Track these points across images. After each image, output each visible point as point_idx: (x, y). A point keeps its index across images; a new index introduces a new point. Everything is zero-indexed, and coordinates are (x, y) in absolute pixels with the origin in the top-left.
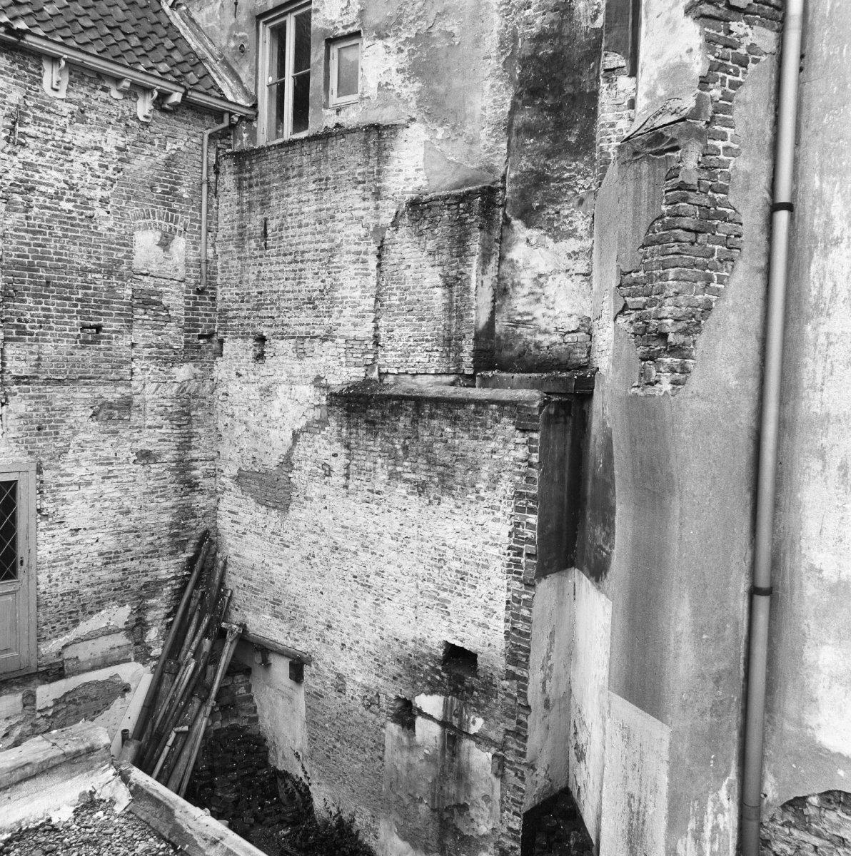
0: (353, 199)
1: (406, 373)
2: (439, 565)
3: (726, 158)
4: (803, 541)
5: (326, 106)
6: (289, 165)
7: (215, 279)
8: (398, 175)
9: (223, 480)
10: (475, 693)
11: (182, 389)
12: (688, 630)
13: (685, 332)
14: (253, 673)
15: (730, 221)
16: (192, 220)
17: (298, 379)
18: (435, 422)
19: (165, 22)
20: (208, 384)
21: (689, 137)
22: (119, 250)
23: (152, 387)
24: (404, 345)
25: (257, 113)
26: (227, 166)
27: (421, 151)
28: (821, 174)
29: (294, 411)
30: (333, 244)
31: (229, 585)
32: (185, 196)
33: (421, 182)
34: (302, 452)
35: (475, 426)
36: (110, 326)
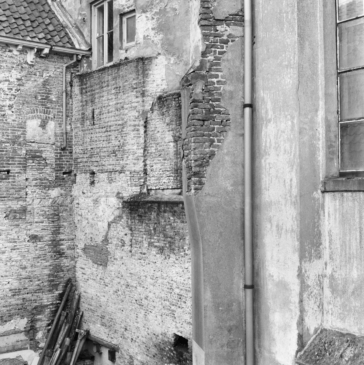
0: (132, 97)
1: (159, 189)
2: (171, 291)
3: (218, 86)
4: (266, 262)
5: (121, 48)
6: (103, 81)
7: (72, 142)
8: (153, 83)
9: (78, 250)
10: (188, 361)
11: (54, 202)
12: (210, 305)
13: (200, 166)
14: (95, 359)
15: (223, 114)
16: (58, 112)
17: (110, 194)
18: (166, 214)
19: (47, 9)
20: (69, 199)
21: (196, 79)
22: (19, 131)
23: (37, 201)
24: (158, 174)
25: (92, 53)
26: (76, 81)
27: (164, 70)
28: (263, 90)
29: (109, 211)
30: (123, 122)
31: (82, 309)
32: (54, 100)
33: (164, 86)
34: (112, 234)
35: (182, 216)
36: (14, 170)
